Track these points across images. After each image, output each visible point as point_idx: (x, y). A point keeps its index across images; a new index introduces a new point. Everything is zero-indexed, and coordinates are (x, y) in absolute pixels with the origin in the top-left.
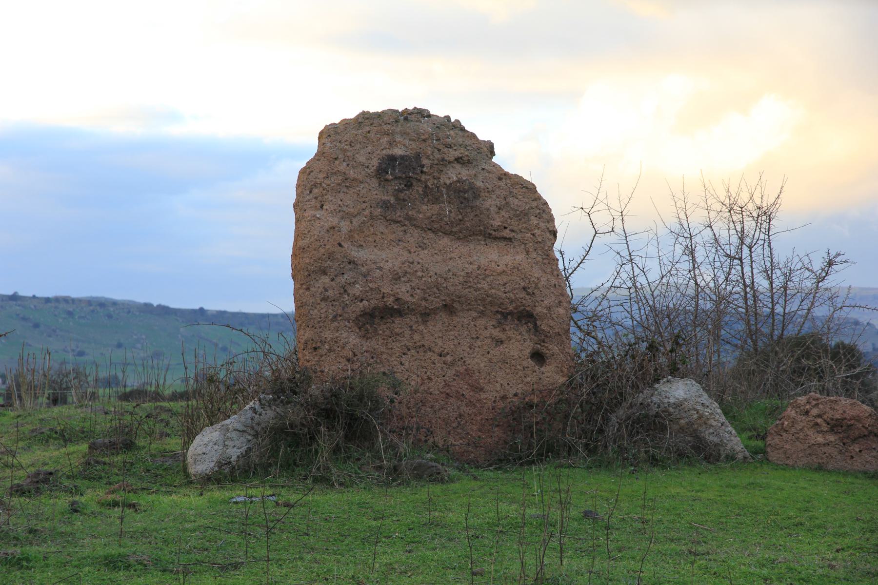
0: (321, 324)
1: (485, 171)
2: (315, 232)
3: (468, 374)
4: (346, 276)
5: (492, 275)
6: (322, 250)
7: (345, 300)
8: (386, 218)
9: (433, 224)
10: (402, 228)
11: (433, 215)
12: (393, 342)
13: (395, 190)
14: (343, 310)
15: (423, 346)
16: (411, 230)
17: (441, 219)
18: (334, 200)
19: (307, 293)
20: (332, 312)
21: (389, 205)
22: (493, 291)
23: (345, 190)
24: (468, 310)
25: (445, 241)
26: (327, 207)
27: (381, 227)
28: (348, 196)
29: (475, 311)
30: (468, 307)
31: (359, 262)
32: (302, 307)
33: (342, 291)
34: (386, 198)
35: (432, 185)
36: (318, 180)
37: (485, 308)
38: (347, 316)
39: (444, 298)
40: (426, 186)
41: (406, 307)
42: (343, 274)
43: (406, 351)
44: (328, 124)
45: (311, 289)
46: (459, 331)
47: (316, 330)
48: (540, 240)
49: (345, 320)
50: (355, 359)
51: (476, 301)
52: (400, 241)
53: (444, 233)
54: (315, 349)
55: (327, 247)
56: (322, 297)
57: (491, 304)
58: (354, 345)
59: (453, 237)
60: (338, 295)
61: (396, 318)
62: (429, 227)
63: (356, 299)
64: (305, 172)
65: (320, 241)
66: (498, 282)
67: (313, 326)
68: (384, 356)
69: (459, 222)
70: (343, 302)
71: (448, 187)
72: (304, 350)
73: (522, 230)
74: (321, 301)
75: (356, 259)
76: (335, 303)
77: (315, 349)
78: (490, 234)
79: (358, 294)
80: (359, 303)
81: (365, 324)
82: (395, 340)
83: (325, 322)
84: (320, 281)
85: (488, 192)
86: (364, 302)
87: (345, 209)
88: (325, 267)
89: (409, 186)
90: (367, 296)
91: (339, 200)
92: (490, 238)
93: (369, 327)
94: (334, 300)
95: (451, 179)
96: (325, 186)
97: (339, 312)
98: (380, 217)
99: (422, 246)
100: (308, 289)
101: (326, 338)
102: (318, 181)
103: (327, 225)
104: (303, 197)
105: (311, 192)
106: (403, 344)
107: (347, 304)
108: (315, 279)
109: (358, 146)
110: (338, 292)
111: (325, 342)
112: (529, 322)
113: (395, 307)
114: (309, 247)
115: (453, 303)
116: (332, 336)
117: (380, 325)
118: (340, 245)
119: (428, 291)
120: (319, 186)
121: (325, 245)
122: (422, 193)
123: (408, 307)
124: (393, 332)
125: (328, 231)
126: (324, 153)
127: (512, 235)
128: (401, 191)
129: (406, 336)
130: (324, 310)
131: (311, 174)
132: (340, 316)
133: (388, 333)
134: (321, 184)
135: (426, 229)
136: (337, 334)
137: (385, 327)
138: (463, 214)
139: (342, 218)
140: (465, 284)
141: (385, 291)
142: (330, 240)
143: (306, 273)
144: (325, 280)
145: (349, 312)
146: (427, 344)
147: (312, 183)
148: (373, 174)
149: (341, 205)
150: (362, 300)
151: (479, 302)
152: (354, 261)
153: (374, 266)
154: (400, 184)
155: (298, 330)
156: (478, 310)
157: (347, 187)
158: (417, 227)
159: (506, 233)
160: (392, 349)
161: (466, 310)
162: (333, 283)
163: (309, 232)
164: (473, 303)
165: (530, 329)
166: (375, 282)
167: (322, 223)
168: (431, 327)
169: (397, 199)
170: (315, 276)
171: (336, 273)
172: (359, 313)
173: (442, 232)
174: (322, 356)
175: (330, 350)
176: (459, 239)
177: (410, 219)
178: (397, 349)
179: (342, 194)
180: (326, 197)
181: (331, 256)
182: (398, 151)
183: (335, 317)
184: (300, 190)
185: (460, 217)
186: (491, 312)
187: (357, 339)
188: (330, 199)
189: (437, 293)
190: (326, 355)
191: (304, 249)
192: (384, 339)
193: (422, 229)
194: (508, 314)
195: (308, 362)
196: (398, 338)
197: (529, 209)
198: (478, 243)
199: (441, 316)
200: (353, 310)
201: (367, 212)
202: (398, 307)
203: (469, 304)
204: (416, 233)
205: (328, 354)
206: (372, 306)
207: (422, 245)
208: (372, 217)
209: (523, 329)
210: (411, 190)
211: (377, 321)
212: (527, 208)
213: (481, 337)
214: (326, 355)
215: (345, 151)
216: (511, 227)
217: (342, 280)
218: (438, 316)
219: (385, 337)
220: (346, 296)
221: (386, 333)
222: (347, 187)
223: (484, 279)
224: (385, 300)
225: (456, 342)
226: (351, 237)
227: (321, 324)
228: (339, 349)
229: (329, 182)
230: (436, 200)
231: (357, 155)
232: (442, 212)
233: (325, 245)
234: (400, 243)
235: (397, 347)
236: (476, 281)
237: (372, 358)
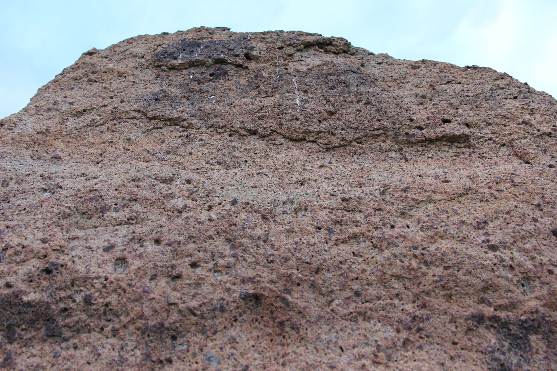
8: (145, 115)
22: (445, 245)
24: (353, 318)
29: (385, 320)
30: (352, 307)
37: (424, 306)
39: (251, 273)
41: (79, 298)
44: (102, 45)
51: (383, 281)
53: (292, 140)
59: (315, 146)
61: (27, 344)
66: (455, 219)
69: (326, 116)
115: (288, 291)
119: (191, 246)
123: (88, 301)
135: (242, 132)
140: (337, 229)
151: (397, 285)
156: (396, 315)
161: (344, 317)
164: (372, 291)
173: (284, 137)
186: (453, 320)
189: (223, 256)
197: (491, 89)
198: (382, 157)
199: (233, 340)
202: (45, 297)
203: (357, 294)
218: (220, 339)
236: (376, 220)
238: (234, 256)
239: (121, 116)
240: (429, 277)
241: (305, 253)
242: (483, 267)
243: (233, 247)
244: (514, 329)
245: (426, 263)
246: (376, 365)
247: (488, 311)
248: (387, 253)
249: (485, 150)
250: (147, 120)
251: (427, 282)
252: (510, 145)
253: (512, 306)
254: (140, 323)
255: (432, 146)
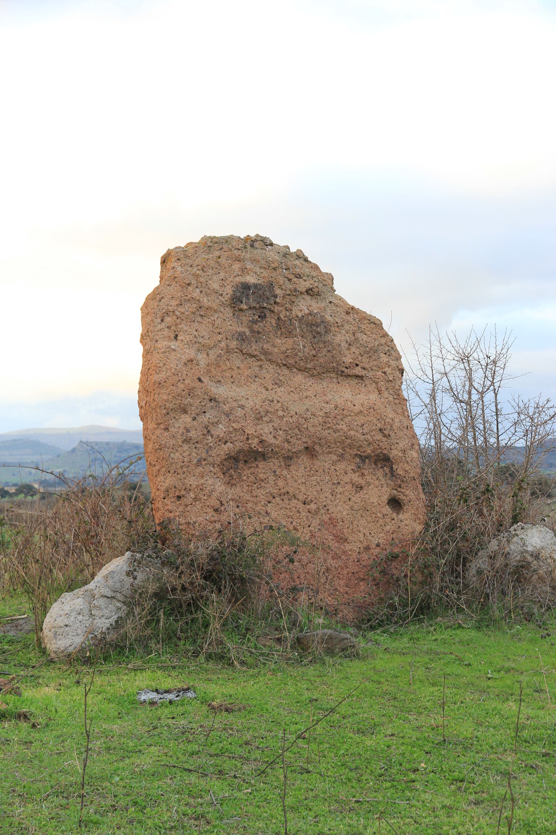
0: (185, 469)
1: (332, 304)
2: (172, 365)
3: (332, 523)
4: (207, 415)
5: (350, 415)
6: (181, 386)
7: (209, 441)
8: (242, 352)
9: (287, 359)
10: (258, 363)
11: (287, 350)
12: (258, 489)
13: (250, 321)
14: (207, 453)
15: (288, 493)
16: (267, 365)
17: (296, 355)
18: (189, 330)
19: (166, 434)
20: (196, 455)
21: (244, 337)
22: (352, 433)
23: (200, 319)
25: (299, 378)
26: (183, 338)
27: (237, 361)
28: (204, 326)
29: (335, 454)
31: (220, 400)
32: (161, 449)
33: (205, 431)
34: (240, 329)
35: (284, 317)
36: (170, 308)
37: (344, 450)
38: (211, 460)
40: (279, 318)
41: (270, 450)
42: (204, 412)
43: (271, 498)
45: (170, 429)
46: (320, 476)
47: (179, 476)
48: (391, 379)
49: (210, 465)
50: (222, 509)
51: (335, 443)
52: (256, 377)
54: (179, 497)
55: (187, 382)
56: (184, 438)
57: (351, 446)
58: (220, 493)
59: (307, 374)
60: (202, 437)
62: (284, 362)
63: (220, 441)
64: (155, 298)
65: (178, 375)
66: (356, 423)
67: (175, 472)
68: (250, 505)
70: (207, 444)
71: (301, 320)
72: (164, 499)
73: (373, 368)
74: (183, 443)
75: (217, 396)
76: (198, 446)
77: (179, 497)
78: (343, 372)
79: (222, 436)
80: (223, 446)
81: (229, 469)
82: (259, 486)
83: (188, 467)
84: (180, 421)
85: (338, 326)
86: (228, 444)
87: (200, 340)
88: (185, 405)
89: (263, 317)
90: (231, 437)
91: (194, 331)
92: (342, 375)
93: (233, 473)
94: (197, 442)
95: (303, 312)
96: (179, 314)
97: (204, 455)
98: (236, 350)
99: (278, 383)
100: (167, 429)
101: (190, 485)
102: (171, 308)
103: (184, 358)
104: (154, 326)
105: (162, 321)
106: (268, 491)
107: (210, 447)
108: (174, 417)
109: (210, 272)
110: (201, 433)
111: (190, 490)
112: (385, 466)
113: (260, 450)
114: (165, 382)
116: (197, 483)
117: (244, 470)
118: (200, 380)
119: (290, 432)
120: (171, 313)
121: (184, 380)
122: (275, 325)
123: (272, 450)
124: (258, 478)
125: (186, 364)
126: (175, 277)
127: (364, 373)
128: (255, 322)
129: (270, 482)
130: (187, 453)
131: (162, 300)
132: (205, 460)
133: (252, 478)
134: (174, 312)
136: (203, 481)
137: (249, 471)
138: (317, 349)
139: (198, 350)
141: (249, 433)
142: (189, 374)
143: (164, 411)
144: (186, 419)
145: (213, 455)
146: (291, 490)
147: (164, 311)
148: (228, 303)
149: (197, 336)
150: (226, 442)
151: (338, 444)
152: (215, 398)
153: (235, 404)
154: (254, 315)
155: (156, 476)
156: (338, 453)
157: (201, 316)
158: (273, 362)
159: (358, 371)
160: (257, 497)
162: (195, 423)
163: (164, 364)
165: (386, 474)
166: (239, 422)
167: (179, 355)
168: (294, 472)
169: (252, 331)
170: (175, 415)
171: (197, 411)
172: (223, 457)
173: (296, 368)
174: (186, 506)
175: (196, 499)
176: (313, 376)
177: (265, 353)
178: (262, 497)
179: (196, 324)
180: (181, 326)
181: (191, 392)
182: (251, 279)
183: (199, 461)
184: (149, 319)
185: (314, 352)
186: (350, 455)
187: (223, 486)
188: (185, 328)
190: (191, 504)
191: (160, 384)
192: (248, 486)
193: (278, 365)
194: (366, 457)
195: (171, 512)
196: (263, 484)
197: (378, 345)
198: (330, 381)
200: (218, 453)
201: (223, 344)
204: (271, 368)
205: (194, 503)
206: (237, 449)
207: (278, 382)
208: (228, 351)
209: (380, 473)
210: (264, 322)
211: (241, 465)
212: (377, 344)
213: (342, 483)
214: (191, 504)
215: (197, 276)
216: (362, 364)
217: (204, 419)
218: (301, 460)
219: (250, 484)
220: (210, 437)
221: (250, 479)
222: (201, 316)
223: (342, 420)
224: (250, 441)
225: (318, 488)
226: (209, 371)
227: (185, 469)
228: (205, 498)
229: (183, 310)
230: (290, 334)
231: (210, 282)
232: (296, 347)
233: (184, 380)
234: (257, 379)
235: (260, 493)
237: (238, 507)
238: (301, 435)
239: (231, 350)
240: (347, 443)
241: (318, 434)
242: (360, 440)
243: (300, 431)
244: (363, 458)
245: (347, 438)
246: (254, 443)
247: (359, 453)
248: (337, 434)
249: (368, 383)
250: (241, 354)
251: (346, 444)
252: (377, 383)
253: (364, 452)
254: (283, 456)
255: (349, 378)
